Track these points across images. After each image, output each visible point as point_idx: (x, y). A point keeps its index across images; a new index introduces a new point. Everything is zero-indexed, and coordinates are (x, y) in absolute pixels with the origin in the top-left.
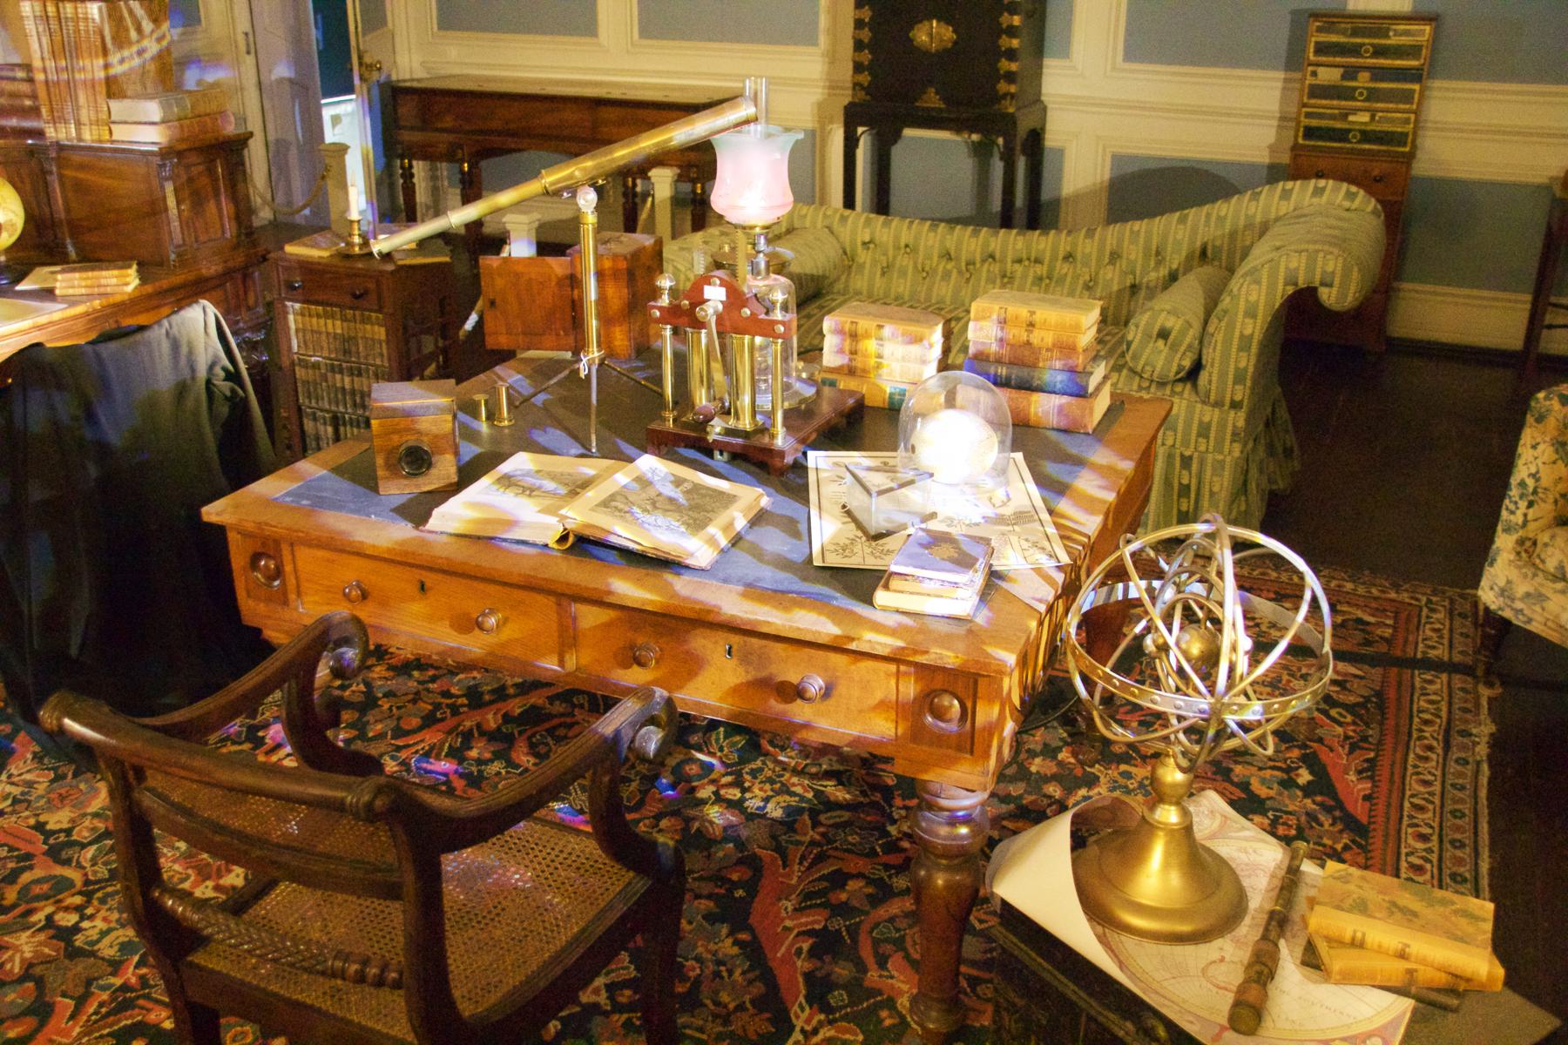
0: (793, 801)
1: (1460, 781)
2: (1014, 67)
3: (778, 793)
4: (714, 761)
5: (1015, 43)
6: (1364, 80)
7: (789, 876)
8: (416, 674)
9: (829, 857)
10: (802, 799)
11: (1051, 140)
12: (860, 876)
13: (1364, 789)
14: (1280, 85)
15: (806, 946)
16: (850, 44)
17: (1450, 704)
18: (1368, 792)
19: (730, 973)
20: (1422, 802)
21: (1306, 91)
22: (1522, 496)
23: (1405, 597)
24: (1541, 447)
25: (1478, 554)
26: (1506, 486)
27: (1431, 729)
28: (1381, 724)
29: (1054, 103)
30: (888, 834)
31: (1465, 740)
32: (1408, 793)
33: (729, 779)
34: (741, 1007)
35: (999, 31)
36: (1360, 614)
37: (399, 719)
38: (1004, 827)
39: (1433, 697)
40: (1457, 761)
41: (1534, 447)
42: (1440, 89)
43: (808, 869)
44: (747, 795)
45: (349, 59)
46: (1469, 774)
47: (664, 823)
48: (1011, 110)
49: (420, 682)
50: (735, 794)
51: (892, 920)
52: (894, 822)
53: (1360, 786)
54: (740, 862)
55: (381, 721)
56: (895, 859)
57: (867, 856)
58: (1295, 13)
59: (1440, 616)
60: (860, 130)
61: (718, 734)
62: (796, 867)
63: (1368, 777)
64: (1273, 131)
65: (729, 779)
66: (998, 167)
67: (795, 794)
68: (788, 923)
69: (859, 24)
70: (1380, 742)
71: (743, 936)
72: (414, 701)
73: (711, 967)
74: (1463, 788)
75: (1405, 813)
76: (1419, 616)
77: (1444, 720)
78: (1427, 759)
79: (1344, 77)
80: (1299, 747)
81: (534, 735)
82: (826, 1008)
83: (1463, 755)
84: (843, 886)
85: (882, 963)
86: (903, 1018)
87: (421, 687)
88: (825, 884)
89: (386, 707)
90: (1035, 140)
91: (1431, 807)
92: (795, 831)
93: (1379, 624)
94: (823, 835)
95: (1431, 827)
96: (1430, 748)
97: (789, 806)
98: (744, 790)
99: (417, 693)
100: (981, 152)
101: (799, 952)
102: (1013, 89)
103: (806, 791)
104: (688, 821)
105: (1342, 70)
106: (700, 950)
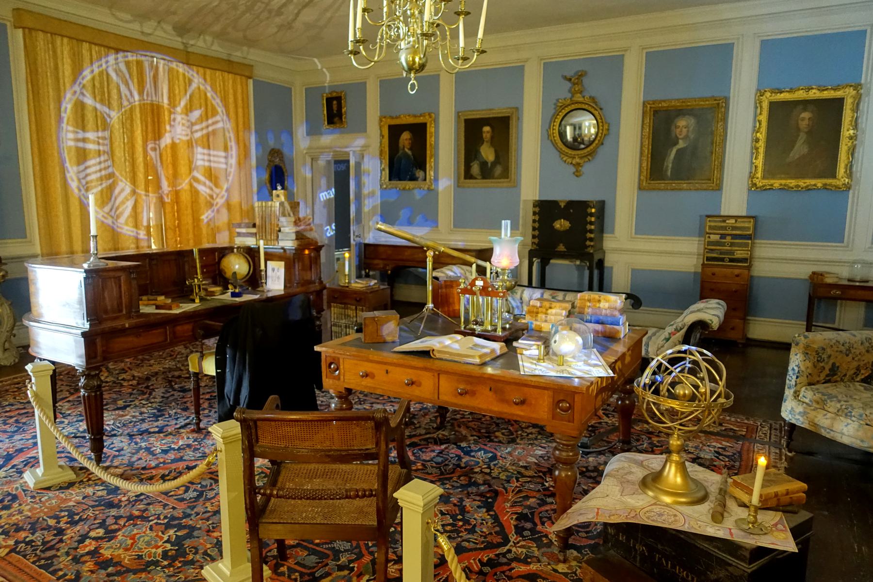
0: (509, 474)
2: (592, 236)
3: (503, 471)
5: (593, 227)
6: (729, 239)
7: (509, 496)
10: (512, 473)
11: (607, 264)
12: (534, 497)
14: (696, 245)
15: (514, 517)
16: (531, 228)
19: (487, 523)
22: (793, 374)
23: (752, 422)
24: (798, 355)
25: (778, 399)
26: (787, 370)
34: (491, 534)
35: (587, 223)
36: (732, 427)
41: (796, 355)
47: (462, 478)
48: (591, 251)
50: (488, 471)
51: (547, 511)
52: (547, 482)
54: (489, 491)
56: (547, 493)
58: (701, 216)
60: (534, 259)
65: (485, 466)
68: (508, 510)
69: (534, 221)
70: (740, 468)
71: (491, 513)
73: (480, 521)
76: (757, 429)
79: (721, 238)
82: (523, 536)
84: (528, 500)
85: (543, 524)
86: (551, 541)
88: (521, 499)
90: (601, 264)
93: (739, 431)
98: (491, 470)
100: (579, 268)
101: (512, 519)
102: (592, 244)
104: (471, 478)
106: (476, 516)
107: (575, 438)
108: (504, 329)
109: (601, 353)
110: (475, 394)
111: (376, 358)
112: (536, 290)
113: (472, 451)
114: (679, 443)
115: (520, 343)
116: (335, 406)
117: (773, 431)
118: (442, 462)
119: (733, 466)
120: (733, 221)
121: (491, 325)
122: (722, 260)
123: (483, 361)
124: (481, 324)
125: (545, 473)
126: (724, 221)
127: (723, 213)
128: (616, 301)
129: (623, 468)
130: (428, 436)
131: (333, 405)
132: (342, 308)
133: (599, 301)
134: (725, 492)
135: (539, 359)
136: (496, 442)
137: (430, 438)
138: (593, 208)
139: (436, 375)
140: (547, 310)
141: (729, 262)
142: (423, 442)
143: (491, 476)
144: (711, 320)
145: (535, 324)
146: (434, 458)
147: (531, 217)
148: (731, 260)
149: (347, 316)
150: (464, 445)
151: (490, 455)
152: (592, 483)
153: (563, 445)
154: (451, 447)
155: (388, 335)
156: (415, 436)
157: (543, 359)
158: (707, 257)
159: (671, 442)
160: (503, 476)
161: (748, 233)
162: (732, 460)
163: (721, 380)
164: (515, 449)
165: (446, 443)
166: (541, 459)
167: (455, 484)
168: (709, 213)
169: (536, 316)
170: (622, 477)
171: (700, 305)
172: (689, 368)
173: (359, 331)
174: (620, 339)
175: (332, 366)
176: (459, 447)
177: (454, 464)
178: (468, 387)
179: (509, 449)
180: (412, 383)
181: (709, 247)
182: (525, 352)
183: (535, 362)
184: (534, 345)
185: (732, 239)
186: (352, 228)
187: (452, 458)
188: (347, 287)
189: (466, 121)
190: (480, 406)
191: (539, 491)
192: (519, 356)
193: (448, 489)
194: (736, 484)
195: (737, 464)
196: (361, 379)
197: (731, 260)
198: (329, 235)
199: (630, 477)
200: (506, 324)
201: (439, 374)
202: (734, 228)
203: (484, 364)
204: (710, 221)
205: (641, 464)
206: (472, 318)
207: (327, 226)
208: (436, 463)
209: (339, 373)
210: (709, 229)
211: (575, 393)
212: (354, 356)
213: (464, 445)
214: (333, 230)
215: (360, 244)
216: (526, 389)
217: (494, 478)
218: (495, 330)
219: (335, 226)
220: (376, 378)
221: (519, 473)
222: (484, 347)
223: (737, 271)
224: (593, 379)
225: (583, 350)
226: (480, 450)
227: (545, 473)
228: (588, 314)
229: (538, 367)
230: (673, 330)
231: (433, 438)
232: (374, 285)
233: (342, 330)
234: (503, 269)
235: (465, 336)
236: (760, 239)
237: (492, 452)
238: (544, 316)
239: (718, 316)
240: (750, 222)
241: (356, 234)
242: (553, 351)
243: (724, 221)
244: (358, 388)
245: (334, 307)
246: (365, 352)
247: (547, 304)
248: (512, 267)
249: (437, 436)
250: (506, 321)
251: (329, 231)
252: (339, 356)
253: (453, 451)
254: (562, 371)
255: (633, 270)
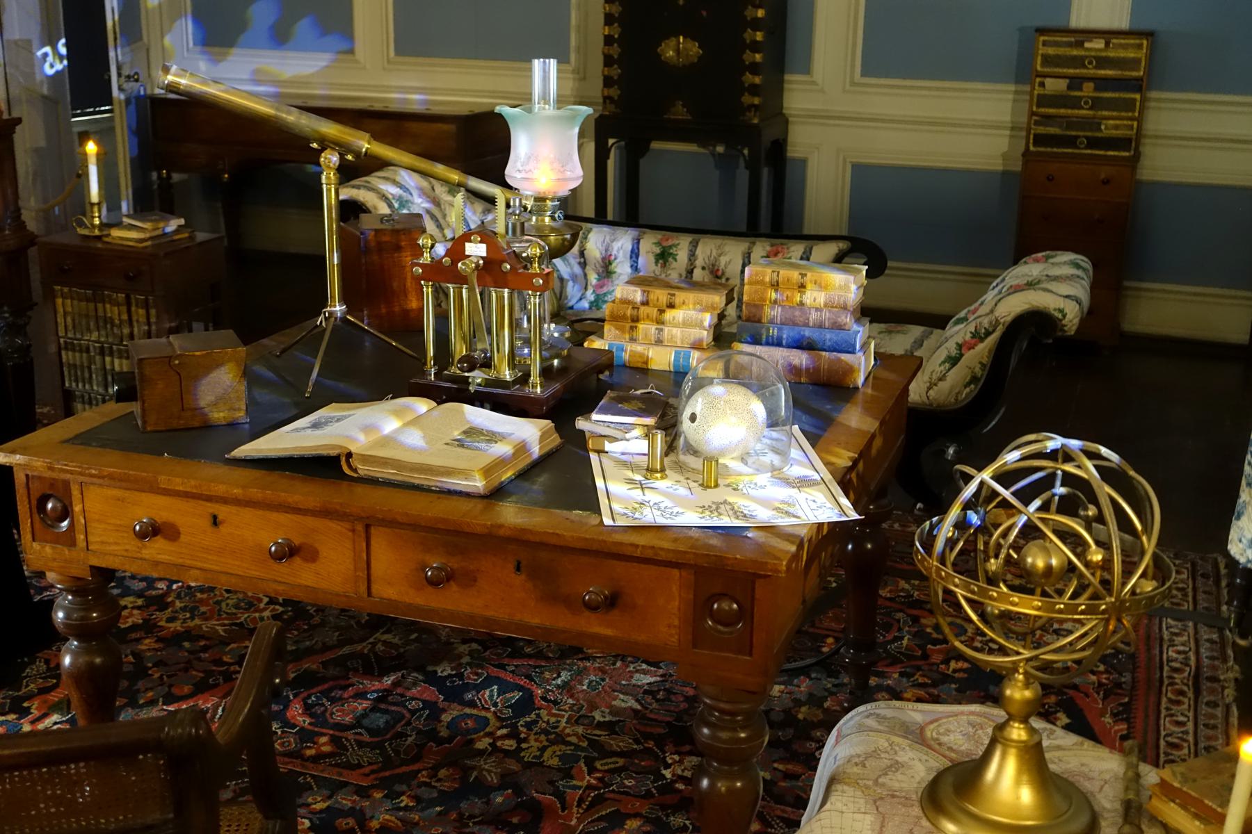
0: (568, 750)
1: (1212, 722)
3: (552, 743)
4: (489, 715)
5: (758, 57)
6: (1088, 90)
8: (187, 644)
9: (606, 799)
10: (577, 747)
12: (636, 815)
13: (1122, 730)
14: (1010, 105)
17: (1197, 653)
18: (1125, 732)
20: (1176, 741)
21: (1035, 100)
27: (1182, 676)
28: (1133, 672)
29: (795, 116)
30: (664, 777)
31: (1215, 685)
32: (1163, 733)
33: (504, 731)
37: (170, 686)
38: (775, 769)
39: (1181, 648)
40: (1208, 704)
42: (1158, 100)
43: (586, 810)
44: (524, 745)
45: (108, 69)
46: (1220, 715)
47: (443, 773)
48: (756, 121)
49: (190, 652)
50: (510, 744)
52: (667, 766)
53: (1116, 728)
55: (151, 689)
57: (643, 797)
58: (1022, 30)
59: (1184, 576)
60: (611, 141)
61: (492, 691)
62: (575, 809)
63: (1122, 720)
64: (1006, 141)
65: (504, 731)
66: (743, 175)
67: (569, 744)
69: (608, 40)
70: (1133, 688)
72: (186, 670)
74: (1214, 727)
75: (1162, 751)
77: (1193, 668)
78: (1179, 703)
79: (1070, 87)
80: (1057, 694)
81: (309, 697)
83: (1212, 698)
87: (192, 657)
89: (157, 676)
90: (779, 146)
91: (1185, 745)
92: (572, 778)
94: (600, 780)
95: (1186, 716)
96: (1182, 693)
97: (564, 754)
98: (520, 741)
99: (189, 662)
100: (727, 164)
102: (756, 101)
103: (580, 740)
104: (467, 770)
105: (1068, 81)
107: (754, 693)
108: (546, 372)
109: (814, 440)
110: (475, 581)
111: (178, 484)
112: (620, 231)
113: (467, 687)
114: (1028, 694)
115: (596, 422)
116: (67, 617)
117: (1200, 581)
118: (389, 726)
119: (1119, 685)
120: (1099, 44)
121: (512, 365)
122: (1071, 142)
123: (496, 483)
124: (487, 364)
125: (660, 741)
126: (1080, 44)
127: (1078, 20)
128: (846, 287)
129: (875, 754)
130: (346, 650)
131: (61, 615)
132: (88, 300)
133: (802, 286)
134: (1140, 808)
135: (650, 470)
136: (529, 656)
137: (352, 656)
138: (760, 7)
139: (360, 528)
140: (662, 311)
141: (1089, 146)
142: (333, 671)
143: (521, 761)
144: (1061, 311)
145: (629, 351)
146: (365, 715)
147: (599, 30)
148: (1094, 143)
149: (104, 322)
150: (444, 670)
151: (517, 695)
152: (781, 760)
153: (722, 712)
154: (410, 680)
155: (215, 404)
156: (310, 652)
157: (663, 470)
158: (1035, 135)
159: (1008, 692)
160: (551, 759)
161: (1135, 74)
162: (1113, 667)
163: (1147, 528)
164: (581, 673)
165: (395, 669)
166: (649, 698)
167: (424, 793)
168: (1040, 23)
169: (632, 328)
170: (876, 782)
171: (1030, 269)
172: (1062, 497)
173: (127, 394)
174: (856, 388)
175: (50, 506)
176: (432, 679)
177: (419, 732)
178: (454, 563)
179: (565, 676)
180: (288, 552)
181: (1042, 110)
182: (608, 446)
183: (638, 477)
184: (633, 426)
185: (1096, 89)
186: (112, 54)
187: (413, 712)
188: (99, 238)
189: (399, 52)
190: (490, 613)
191: (648, 795)
192: (593, 457)
193: (406, 808)
194: (1165, 789)
195: (1126, 678)
196: (137, 542)
197: (1094, 143)
198: (49, 71)
199: (897, 781)
200: (553, 358)
201: (368, 527)
202: (1102, 62)
203: (497, 493)
204: (1045, 44)
205: (918, 736)
206: (459, 349)
207: (43, 46)
208: (369, 730)
209: (72, 525)
210: (1043, 65)
211: (756, 576)
212: (111, 477)
213: (444, 670)
214: (61, 58)
215: (139, 98)
216: (620, 567)
217: (529, 765)
218: (524, 379)
219: (67, 45)
220: (183, 538)
221: (593, 743)
222: (493, 437)
223: (1104, 172)
224: (803, 532)
225: (767, 432)
226: (488, 683)
227: (660, 741)
228: (771, 322)
229: (651, 496)
230: (968, 336)
231: (361, 655)
232: (177, 232)
233: (91, 361)
234: (540, 199)
235: (440, 402)
236: (1161, 89)
237: (520, 688)
238: (653, 329)
239: (1078, 301)
240: (1140, 46)
241: (126, 72)
242: (686, 441)
243: (1080, 44)
244: (132, 568)
245: (64, 297)
246: (143, 466)
247: (660, 295)
248: (564, 191)
249: (372, 650)
250: (550, 348)
251: (50, 59)
252: (68, 476)
253: (414, 691)
254: (716, 508)
255: (857, 168)
